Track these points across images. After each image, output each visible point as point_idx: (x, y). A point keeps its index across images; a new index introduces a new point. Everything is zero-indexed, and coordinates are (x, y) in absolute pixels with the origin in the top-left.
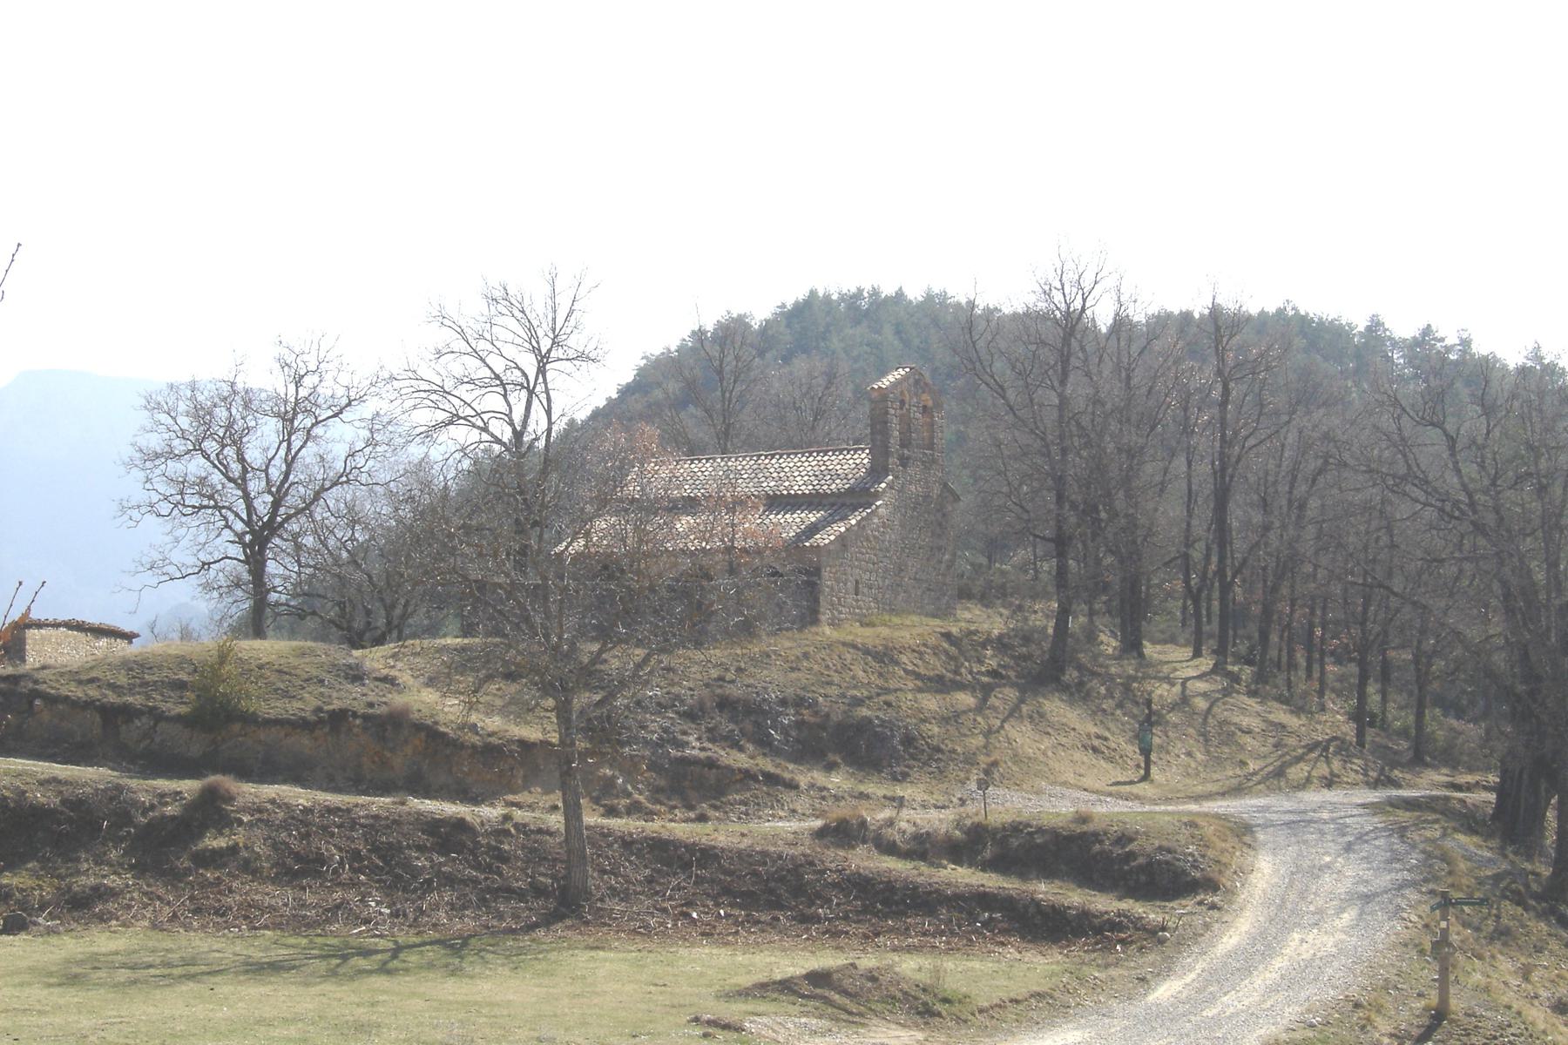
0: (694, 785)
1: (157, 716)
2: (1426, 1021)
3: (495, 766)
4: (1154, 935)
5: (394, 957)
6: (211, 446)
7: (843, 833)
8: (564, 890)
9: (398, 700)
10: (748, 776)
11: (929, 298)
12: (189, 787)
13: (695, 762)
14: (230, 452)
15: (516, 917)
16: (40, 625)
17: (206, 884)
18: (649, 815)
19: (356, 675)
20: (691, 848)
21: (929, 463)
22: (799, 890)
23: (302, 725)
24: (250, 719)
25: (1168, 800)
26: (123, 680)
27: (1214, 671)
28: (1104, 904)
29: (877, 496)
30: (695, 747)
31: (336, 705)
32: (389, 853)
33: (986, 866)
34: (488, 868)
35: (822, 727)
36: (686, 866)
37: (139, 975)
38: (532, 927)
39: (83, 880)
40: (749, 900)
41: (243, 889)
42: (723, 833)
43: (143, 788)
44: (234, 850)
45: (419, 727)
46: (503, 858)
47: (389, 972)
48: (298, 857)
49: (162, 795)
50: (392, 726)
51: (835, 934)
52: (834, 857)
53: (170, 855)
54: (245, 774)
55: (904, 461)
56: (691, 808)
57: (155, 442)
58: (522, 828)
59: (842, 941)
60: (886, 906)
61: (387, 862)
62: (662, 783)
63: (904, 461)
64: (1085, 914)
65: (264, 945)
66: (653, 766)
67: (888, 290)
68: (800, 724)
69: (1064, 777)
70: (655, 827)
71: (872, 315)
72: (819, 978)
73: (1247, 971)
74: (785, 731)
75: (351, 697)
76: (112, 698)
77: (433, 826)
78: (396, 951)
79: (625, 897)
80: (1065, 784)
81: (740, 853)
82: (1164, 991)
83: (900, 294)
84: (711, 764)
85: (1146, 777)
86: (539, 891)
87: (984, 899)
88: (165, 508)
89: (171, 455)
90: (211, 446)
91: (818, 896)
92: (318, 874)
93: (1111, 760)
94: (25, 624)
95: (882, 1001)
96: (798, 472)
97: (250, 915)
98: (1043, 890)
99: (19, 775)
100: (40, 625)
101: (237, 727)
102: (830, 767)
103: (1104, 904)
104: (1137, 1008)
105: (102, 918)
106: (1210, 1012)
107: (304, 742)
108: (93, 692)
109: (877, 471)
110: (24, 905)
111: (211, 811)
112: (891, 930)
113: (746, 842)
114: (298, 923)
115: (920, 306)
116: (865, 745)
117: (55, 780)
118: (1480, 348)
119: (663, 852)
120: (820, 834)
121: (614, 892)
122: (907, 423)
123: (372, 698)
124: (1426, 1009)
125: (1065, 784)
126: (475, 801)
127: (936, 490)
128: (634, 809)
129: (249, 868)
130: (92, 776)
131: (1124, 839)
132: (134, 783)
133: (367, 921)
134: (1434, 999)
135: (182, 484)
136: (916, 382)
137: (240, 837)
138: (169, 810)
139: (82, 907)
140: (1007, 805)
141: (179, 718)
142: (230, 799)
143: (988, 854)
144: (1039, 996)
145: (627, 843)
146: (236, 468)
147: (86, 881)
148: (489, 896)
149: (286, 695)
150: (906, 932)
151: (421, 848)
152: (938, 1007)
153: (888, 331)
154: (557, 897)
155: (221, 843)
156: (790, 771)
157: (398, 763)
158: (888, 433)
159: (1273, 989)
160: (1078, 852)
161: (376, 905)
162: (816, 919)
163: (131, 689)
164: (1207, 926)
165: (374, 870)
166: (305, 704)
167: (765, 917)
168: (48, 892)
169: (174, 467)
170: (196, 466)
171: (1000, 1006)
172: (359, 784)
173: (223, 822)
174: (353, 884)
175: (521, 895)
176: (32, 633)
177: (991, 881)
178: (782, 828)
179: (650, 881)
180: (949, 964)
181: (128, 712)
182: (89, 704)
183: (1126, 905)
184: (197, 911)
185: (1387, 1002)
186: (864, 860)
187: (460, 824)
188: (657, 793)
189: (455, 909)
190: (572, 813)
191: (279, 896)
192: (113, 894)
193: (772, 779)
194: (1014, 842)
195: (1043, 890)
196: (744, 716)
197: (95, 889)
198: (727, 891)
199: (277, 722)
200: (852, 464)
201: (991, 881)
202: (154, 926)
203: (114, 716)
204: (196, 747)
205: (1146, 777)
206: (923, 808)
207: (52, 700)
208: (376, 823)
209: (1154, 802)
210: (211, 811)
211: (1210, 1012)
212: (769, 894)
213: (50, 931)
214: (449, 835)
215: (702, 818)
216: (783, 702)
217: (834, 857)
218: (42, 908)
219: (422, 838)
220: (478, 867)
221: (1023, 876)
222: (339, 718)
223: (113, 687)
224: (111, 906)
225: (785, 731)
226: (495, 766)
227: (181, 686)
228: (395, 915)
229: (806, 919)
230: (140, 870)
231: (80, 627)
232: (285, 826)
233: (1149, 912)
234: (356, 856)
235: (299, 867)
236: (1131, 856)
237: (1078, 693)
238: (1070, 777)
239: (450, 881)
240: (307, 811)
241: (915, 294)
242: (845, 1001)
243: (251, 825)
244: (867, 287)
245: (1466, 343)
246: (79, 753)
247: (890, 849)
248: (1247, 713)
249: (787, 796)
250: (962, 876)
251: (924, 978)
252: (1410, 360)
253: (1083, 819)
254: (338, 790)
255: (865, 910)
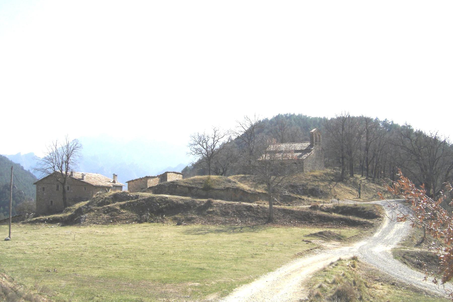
0: (287, 200)
1: (198, 188)
2: (422, 240)
3: (254, 196)
4: (372, 225)
5: (241, 229)
6: (201, 143)
7: (314, 208)
8: (269, 218)
9: (237, 186)
10: (296, 198)
11: (299, 115)
12: (205, 200)
13: (287, 196)
14: (205, 144)
15: (262, 222)
16: (169, 172)
17: (209, 217)
18: (280, 205)
19: (229, 181)
20: (290, 210)
21: (320, 144)
22: (309, 217)
23: (222, 190)
24: (213, 189)
25: (364, 201)
26: (191, 182)
27: (366, 179)
28: (362, 220)
29: (312, 150)
30: (287, 193)
31: (227, 186)
32: (240, 212)
33: (340, 213)
34: (256, 214)
35: (307, 190)
36: (289, 213)
37: (197, 232)
38: (265, 224)
39: (189, 216)
40: (300, 219)
41: (216, 218)
42: (295, 208)
43: (198, 200)
44: (214, 211)
45: (241, 190)
46: (258, 212)
47: (241, 232)
48: (224, 212)
49: (201, 202)
50: (237, 190)
51: (316, 225)
52: (314, 212)
53: (204, 213)
54: (213, 198)
55: (316, 144)
56: (287, 203)
57: (192, 142)
58: (261, 207)
59: (318, 226)
60: (324, 221)
61: (240, 213)
62: (282, 199)
63: (316, 144)
64: (359, 222)
65: (222, 227)
66: (280, 196)
67: (292, 114)
68: (303, 189)
69: (348, 199)
70: (282, 207)
71: (290, 117)
72: (320, 233)
73: (389, 231)
74: (301, 190)
75: (229, 185)
76: (190, 185)
77: (246, 207)
78: (242, 228)
79: (280, 219)
80: (347, 199)
81: (298, 211)
82: (376, 235)
83: (294, 114)
84: (290, 196)
85: (360, 198)
86: (265, 218)
87: (341, 219)
88: (194, 153)
89: (195, 145)
90: (201, 143)
91: (312, 219)
92: (228, 215)
93: (353, 195)
94: (166, 173)
95: (332, 237)
96: (298, 146)
97: (217, 222)
98: (351, 217)
99: (176, 198)
100: (169, 172)
101: (211, 190)
102: (309, 197)
103: (362, 220)
104: (373, 238)
105: (193, 223)
106: (386, 238)
107: (222, 193)
108: (187, 185)
109: (311, 146)
110: (180, 220)
111: (209, 204)
112: (326, 224)
113: (299, 210)
114: (224, 223)
115: (297, 116)
116: (314, 193)
117: (182, 199)
118: (395, 123)
119: (284, 210)
120: (311, 208)
121: (278, 218)
122: (316, 139)
123: (233, 185)
124: (422, 238)
125: (347, 199)
126: (251, 202)
127: (321, 149)
128: (278, 204)
129: (217, 214)
130: (188, 198)
131: (363, 209)
132: (196, 200)
133: (237, 223)
134: (423, 236)
135: (197, 149)
136: (319, 131)
137: (214, 209)
138: (202, 204)
139: (189, 221)
140: (342, 203)
141: (202, 189)
142: (212, 202)
143: (340, 211)
144: (356, 236)
145: (279, 210)
146: (205, 147)
147: (189, 216)
148: (257, 219)
149: (219, 185)
150: (328, 225)
151: (245, 211)
152: (342, 238)
153: (293, 120)
154: (268, 219)
155: (211, 210)
156: (303, 197)
157: (238, 196)
158: (311, 138)
159: (395, 234)
160: (355, 211)
161: (238, 220)
162: (313, 223)
163: (193, 184)
164: (380, 224)
165: (237, 214)
166: (222, 186)
167: (304, 222)
168: (183, 218)
169: (196, 147)
170: (199, 146)
171: (351, 238)
172: (231, 200)
173: (212, 206)
174: (234, 217)
175: (262, 219)
176: (168, 174)
177: (342, 216)
178: (304, 207)
179: (283, 216)
180: (342, 230)
181: (193, 188)
182: (186, 187)
183: (365, 220)
184: (209, 221)
185: (415, 236)
186: (319, 212)
187: (251, 207)
188: (281, 201)
189: (252, 221)
190: (271, 204)
191: (222, 219)
192: (194, 218)
193: (300, 199)
194: (344, 209)
195: (351, 217)
196: (293, 188)
197: (191, 218)
198: (296, 218)
199: (218, 189)
200: (307, 144)
201: (342, 216)
202: (202, 224)
203: (190, 188)
204: (204, 193)
205: (360, 198)
206: (329, 204)
207: (180, 186)
208: (237, 207)
209: (362, 202)
210: (209, 204)
211: (386, 238)
212: (305, 219)
213: (185, 225)
214: (249, 208)
215: (289, 205)
216: (300, 185)
217: (314, 212)
218: (183, 221)
219: (245, 209)
220: (254, 214)
221: (346, 215)
222: (228, 189)
223: (190, 184)
224: (194, 221)
225: (301, 190)
226: (254, 196)
227: (201, 183)
228: (242, 222)
229: (311, 223)
230: (198, 214)
231: (175, 173)
232: (222, 207)
233: (371, 222)
234: (234, 212)
235: (225, 214)
236: (365, 212)
237: (346, 183)
238: (347, 197)
239: (250, 216)
240: (225, 204)
241: (297, 114)
242: (326, 237)
243: (216, 207)
244: (288, 113)
245: (392, 122)
246: (185, 195)
247: (323, 210)
248: (372, 186)
249: (303, 201)
250: (334, 215)
251: (338, 233)
252: (383, 124)
253: (356, 205)
254: (228, 201)
255: (321, 221)
